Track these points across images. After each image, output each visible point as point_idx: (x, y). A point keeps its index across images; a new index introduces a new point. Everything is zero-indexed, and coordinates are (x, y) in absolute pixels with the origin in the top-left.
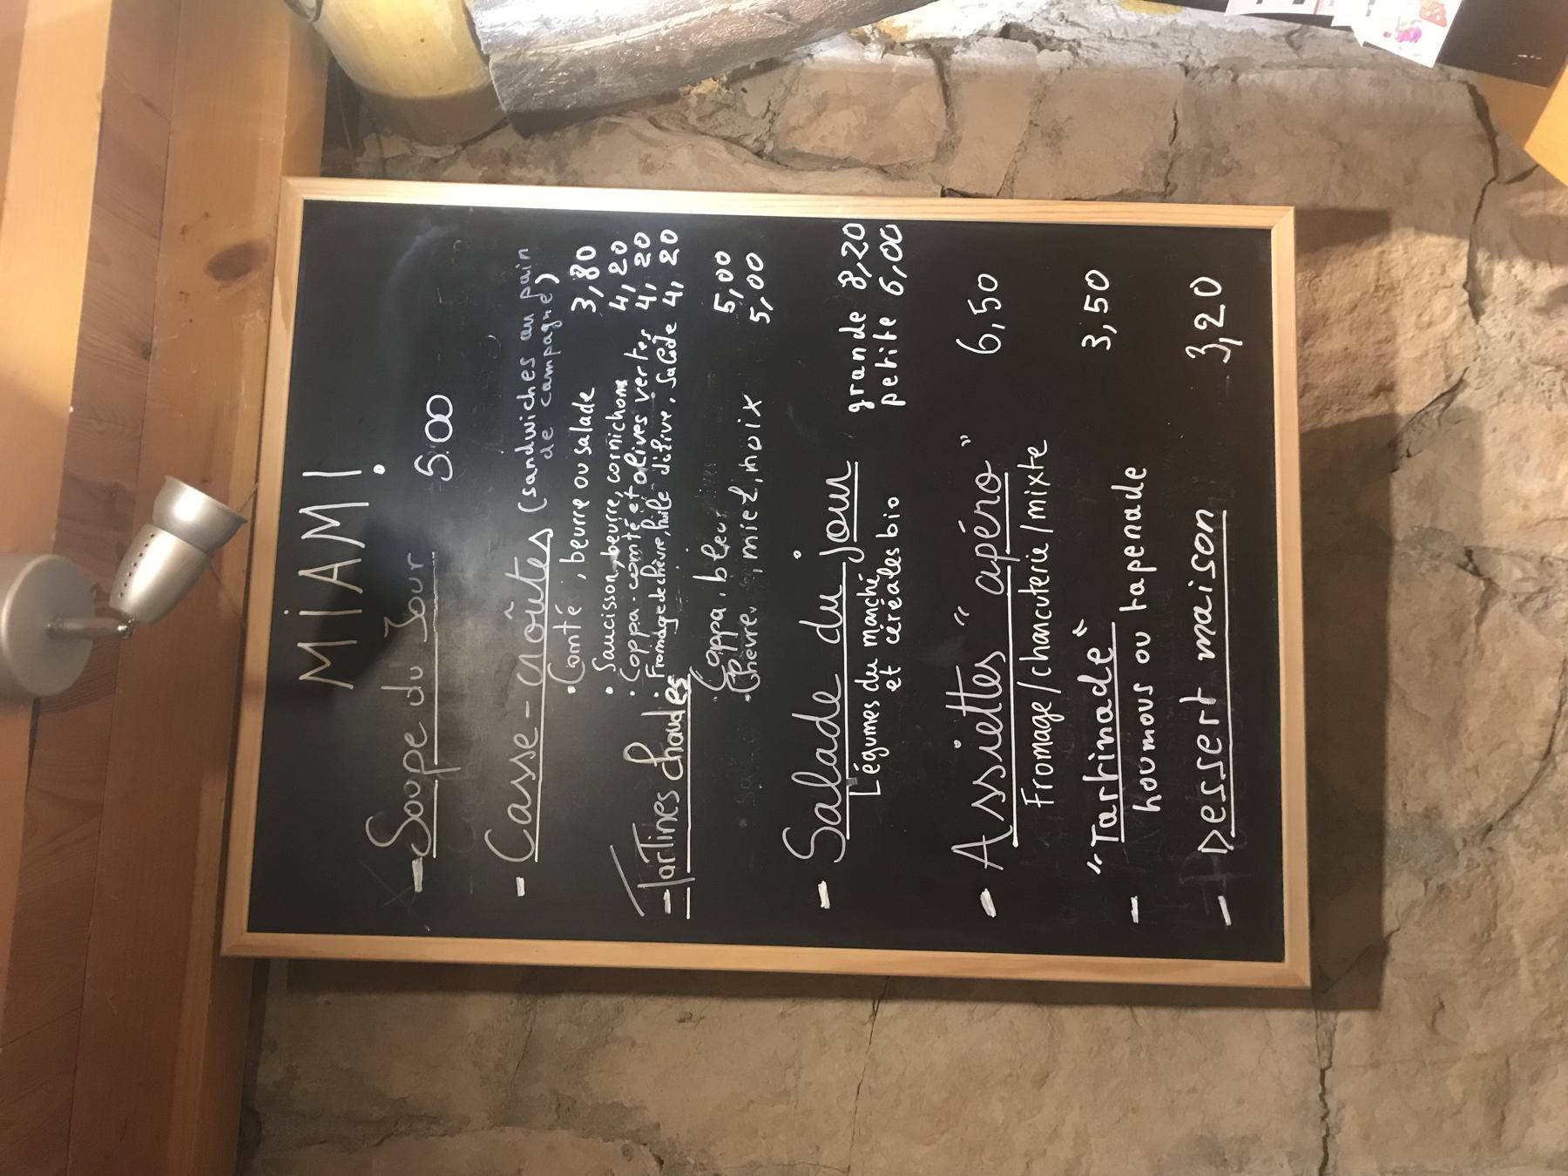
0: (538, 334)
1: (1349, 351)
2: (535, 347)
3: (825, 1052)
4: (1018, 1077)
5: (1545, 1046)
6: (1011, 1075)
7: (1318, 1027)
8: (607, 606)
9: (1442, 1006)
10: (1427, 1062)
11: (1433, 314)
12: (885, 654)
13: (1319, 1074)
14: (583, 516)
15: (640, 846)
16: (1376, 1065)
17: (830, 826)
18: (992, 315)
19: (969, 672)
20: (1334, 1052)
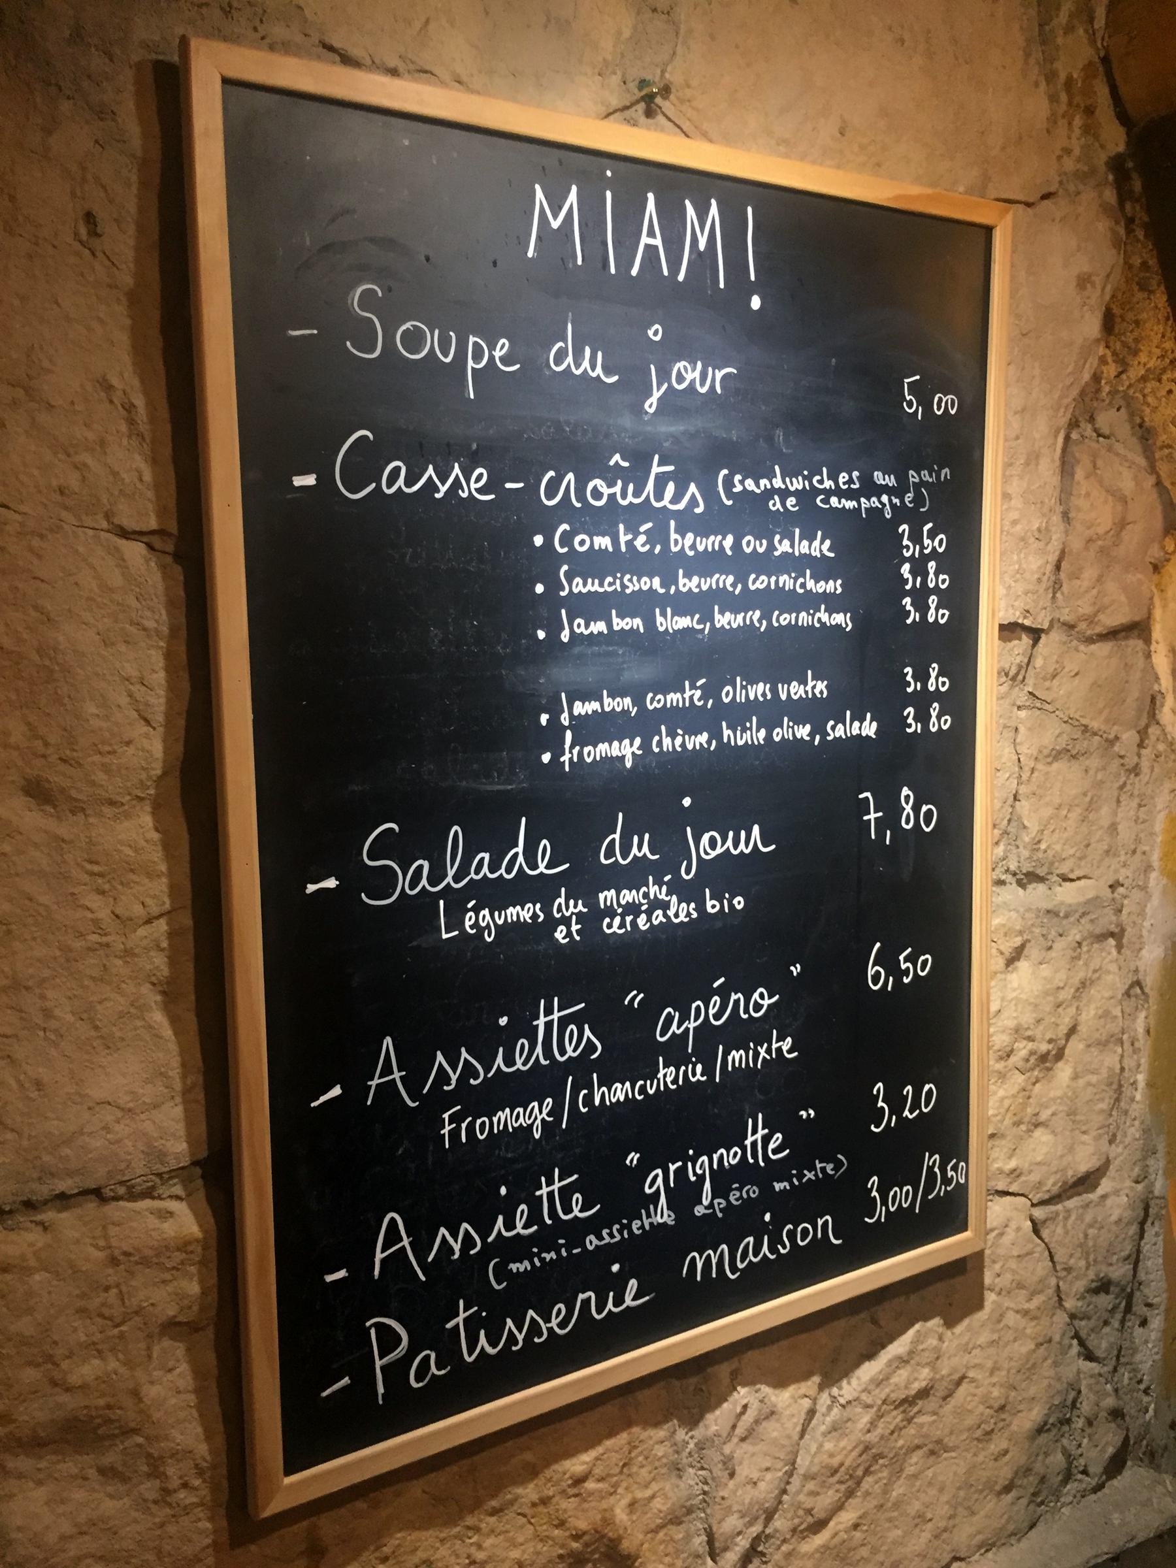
0: (880, 490)
2: (870, 489)
4: (44, 756)
5: (156, 1471)
10: (123, 1328)
12: (593, 917)
16: (114, 1261)
17: (403, 883)
18: (899, 974)
19: (577, 1019)
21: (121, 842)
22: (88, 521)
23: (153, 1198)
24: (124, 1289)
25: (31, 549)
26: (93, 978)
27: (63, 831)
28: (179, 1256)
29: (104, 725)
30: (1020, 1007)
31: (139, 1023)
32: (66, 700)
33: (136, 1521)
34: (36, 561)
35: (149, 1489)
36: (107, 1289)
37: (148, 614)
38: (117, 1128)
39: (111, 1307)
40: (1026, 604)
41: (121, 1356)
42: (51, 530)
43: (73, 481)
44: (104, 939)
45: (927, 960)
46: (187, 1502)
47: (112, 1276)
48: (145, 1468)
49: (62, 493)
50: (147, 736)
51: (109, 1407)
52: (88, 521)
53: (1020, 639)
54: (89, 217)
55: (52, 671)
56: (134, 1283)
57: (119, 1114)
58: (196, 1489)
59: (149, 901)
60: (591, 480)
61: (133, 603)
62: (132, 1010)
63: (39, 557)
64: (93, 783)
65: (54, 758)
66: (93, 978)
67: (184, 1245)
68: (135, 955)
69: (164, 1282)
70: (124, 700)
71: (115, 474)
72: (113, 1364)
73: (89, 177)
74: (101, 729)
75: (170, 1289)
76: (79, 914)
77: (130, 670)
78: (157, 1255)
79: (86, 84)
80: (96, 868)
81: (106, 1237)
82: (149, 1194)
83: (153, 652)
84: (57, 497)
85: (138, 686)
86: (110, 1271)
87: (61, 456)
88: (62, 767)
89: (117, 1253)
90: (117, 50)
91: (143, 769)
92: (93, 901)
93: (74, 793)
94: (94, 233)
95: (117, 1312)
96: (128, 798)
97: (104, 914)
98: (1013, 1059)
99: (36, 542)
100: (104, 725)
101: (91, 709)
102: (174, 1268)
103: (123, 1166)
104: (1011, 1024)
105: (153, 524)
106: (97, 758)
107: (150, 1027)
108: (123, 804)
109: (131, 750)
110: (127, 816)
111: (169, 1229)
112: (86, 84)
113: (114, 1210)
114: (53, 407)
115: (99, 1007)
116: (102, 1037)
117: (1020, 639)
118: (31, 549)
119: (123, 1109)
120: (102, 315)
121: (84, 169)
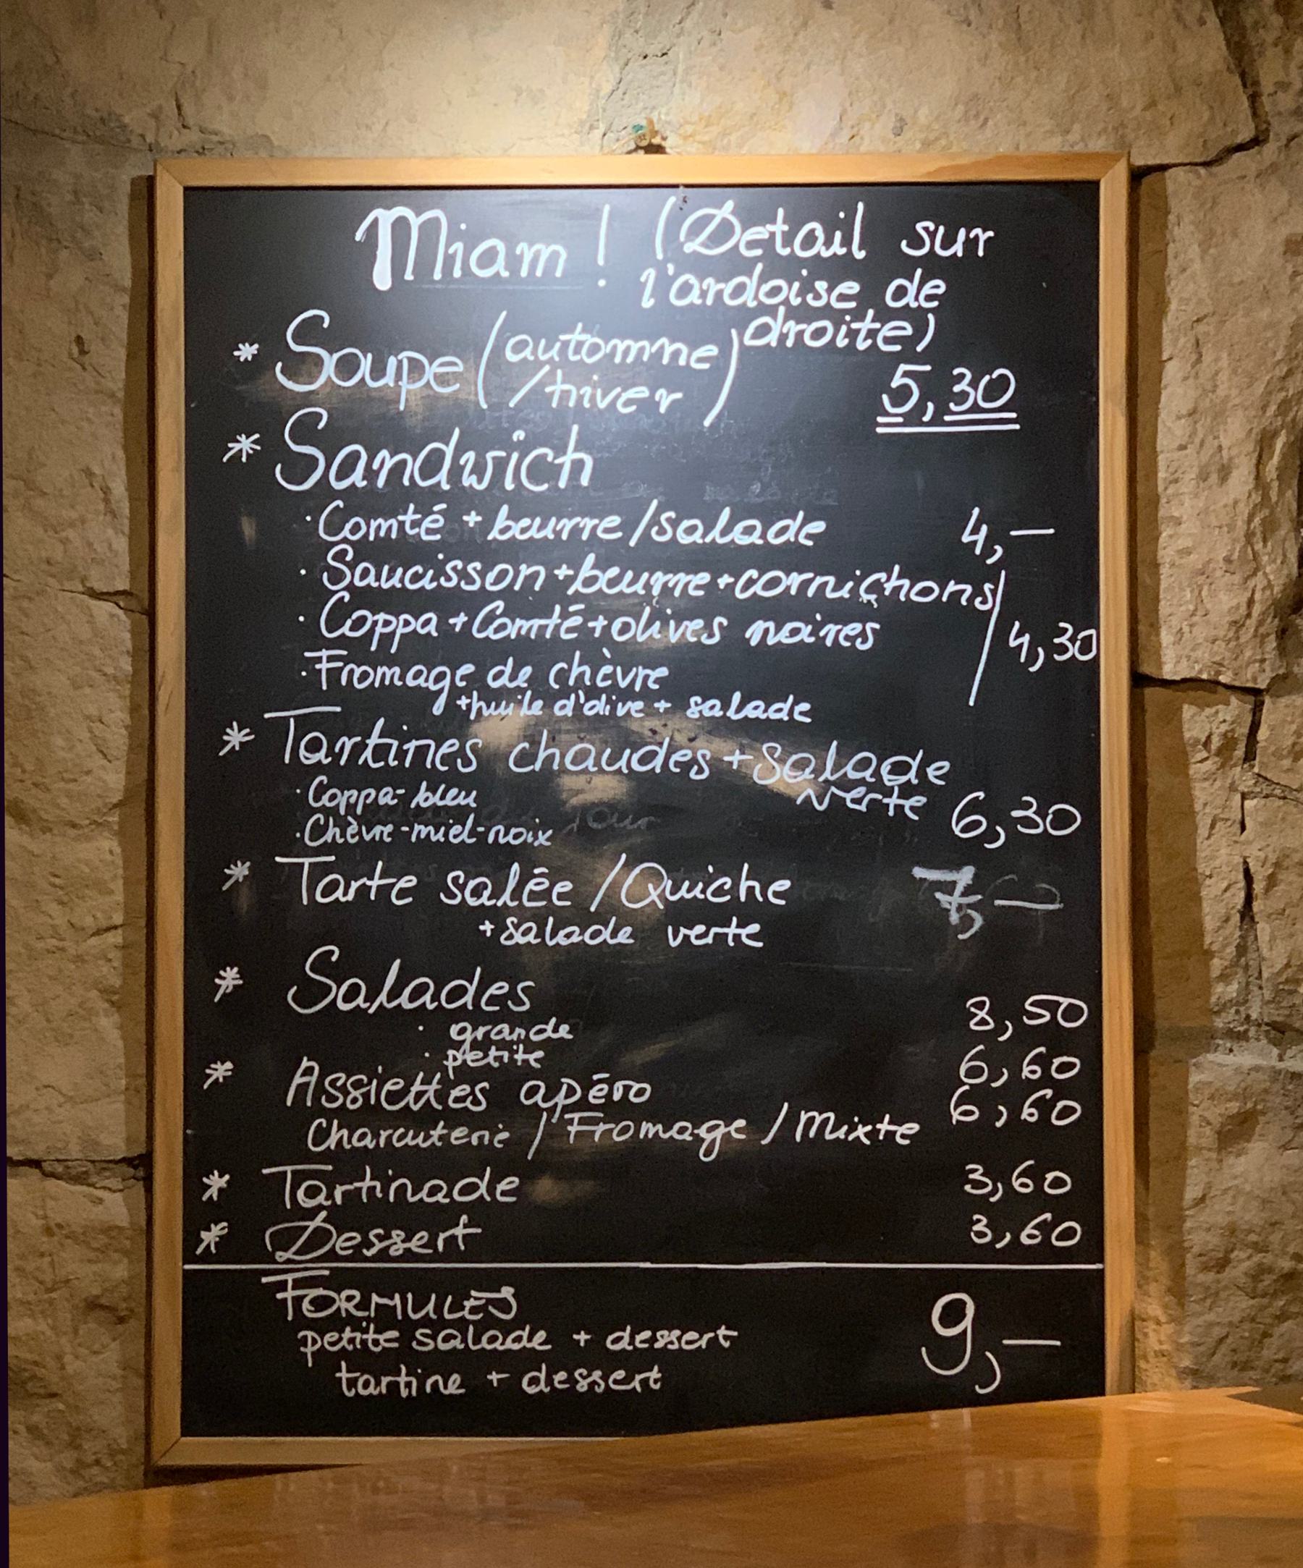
1: (1205, 80)
3: (46, 531)
4: (22, 781)
5: (74, 1444)
6: (24, 771)
7: (93, 1162)
8: (668, 520)
9: (121, 1320)
10: (54, 1295)
11: (1246, 579)
13: (35, 1157)
14: (810, 593)
15: (289, 1169)
16: (48, 1231)
20: (62, 1183)
21: (79, 861)
22: (67, 586)
23: (89, 1185)
24: (55, 1257)
25: (20, 609)
26: (50, 978)
27: (34, 847)
28: (103, 1239)
29: (69, 756)
30: (1241, 1200)
31: (87, 1025)
32: (40, 735)
33: (53, 1485)
34: (25, 619)
35: (68, 1459)
36: (42, 1255)
37: (108, 661)
38: (58, 1110)
39: (44, 1272)
40: (1213, 654)
41: (50, 1321)
42: (38, 594)
43: (58, 554)
44: (61, 944)
45: (1074, 1110)
46: (98, 1479)
47: (45, 1243)
48: (66, 1437)
49: (48, 562)
50: (103, 768)
51: (36, 1363)
52: (67, 586)
53: (1227, 703)
54: (79, 340)
55: (30, 710)
56: (64, 1255)
57: (62, 1100)
58: (107, 1468)
59: (99, 915)
60: (776, 546)
61: (97, 652)
62: (82, 1012)
63: (27, 616)
64: (58, 806)
65: (28, 783)
66: (50, 978)
67: (109, 1230)
68: (83, 961)
69: (89, 1261)
70: (85, 735)
71: (90, 545)
72: (43, 1326)
73: (81, 307)
74: (64, 759)
75: (95, 1268)
76: (42, 919)
77: (92, 710)
78: (84, 1233)
79: (79, 235)
80: (57, 881)
81: (43, 1208)
82: (80, 1179)
83: (111, 694)
84: (44, 566)
85: (98, 724)
86: (45, 1239)
87: (51, 533)
88: (34, 791)
89: (52, 1224)
90: (106, 204)
91: (99, 796)
92: (54, 908)
93: (42, 813)
94: (83, 352)
95: (48, 1277)
96: (87, 822)
97: (60, 921)
98: (1229, 1273)
99: (25, 604)
100: (69, 756)
101: (59, 741)
102: (98, 1249)
103: (59, 1145)
104: (1222, 1220)
105: (122, 584)
106: (62, 785)
107: (96, 1030)
108: (82, 827)
109: (89, 779)
110: (88, 839)
111: (97, 1213)
112: (79, 235)
113: (51, 1184)
114: (45, 494)
115: (52, 1002)
116: (53, 1030)
117: (1227, 703)
118: (20, 609)
119: (64, 1095)
120: (90, 416)
121: (77, 302)
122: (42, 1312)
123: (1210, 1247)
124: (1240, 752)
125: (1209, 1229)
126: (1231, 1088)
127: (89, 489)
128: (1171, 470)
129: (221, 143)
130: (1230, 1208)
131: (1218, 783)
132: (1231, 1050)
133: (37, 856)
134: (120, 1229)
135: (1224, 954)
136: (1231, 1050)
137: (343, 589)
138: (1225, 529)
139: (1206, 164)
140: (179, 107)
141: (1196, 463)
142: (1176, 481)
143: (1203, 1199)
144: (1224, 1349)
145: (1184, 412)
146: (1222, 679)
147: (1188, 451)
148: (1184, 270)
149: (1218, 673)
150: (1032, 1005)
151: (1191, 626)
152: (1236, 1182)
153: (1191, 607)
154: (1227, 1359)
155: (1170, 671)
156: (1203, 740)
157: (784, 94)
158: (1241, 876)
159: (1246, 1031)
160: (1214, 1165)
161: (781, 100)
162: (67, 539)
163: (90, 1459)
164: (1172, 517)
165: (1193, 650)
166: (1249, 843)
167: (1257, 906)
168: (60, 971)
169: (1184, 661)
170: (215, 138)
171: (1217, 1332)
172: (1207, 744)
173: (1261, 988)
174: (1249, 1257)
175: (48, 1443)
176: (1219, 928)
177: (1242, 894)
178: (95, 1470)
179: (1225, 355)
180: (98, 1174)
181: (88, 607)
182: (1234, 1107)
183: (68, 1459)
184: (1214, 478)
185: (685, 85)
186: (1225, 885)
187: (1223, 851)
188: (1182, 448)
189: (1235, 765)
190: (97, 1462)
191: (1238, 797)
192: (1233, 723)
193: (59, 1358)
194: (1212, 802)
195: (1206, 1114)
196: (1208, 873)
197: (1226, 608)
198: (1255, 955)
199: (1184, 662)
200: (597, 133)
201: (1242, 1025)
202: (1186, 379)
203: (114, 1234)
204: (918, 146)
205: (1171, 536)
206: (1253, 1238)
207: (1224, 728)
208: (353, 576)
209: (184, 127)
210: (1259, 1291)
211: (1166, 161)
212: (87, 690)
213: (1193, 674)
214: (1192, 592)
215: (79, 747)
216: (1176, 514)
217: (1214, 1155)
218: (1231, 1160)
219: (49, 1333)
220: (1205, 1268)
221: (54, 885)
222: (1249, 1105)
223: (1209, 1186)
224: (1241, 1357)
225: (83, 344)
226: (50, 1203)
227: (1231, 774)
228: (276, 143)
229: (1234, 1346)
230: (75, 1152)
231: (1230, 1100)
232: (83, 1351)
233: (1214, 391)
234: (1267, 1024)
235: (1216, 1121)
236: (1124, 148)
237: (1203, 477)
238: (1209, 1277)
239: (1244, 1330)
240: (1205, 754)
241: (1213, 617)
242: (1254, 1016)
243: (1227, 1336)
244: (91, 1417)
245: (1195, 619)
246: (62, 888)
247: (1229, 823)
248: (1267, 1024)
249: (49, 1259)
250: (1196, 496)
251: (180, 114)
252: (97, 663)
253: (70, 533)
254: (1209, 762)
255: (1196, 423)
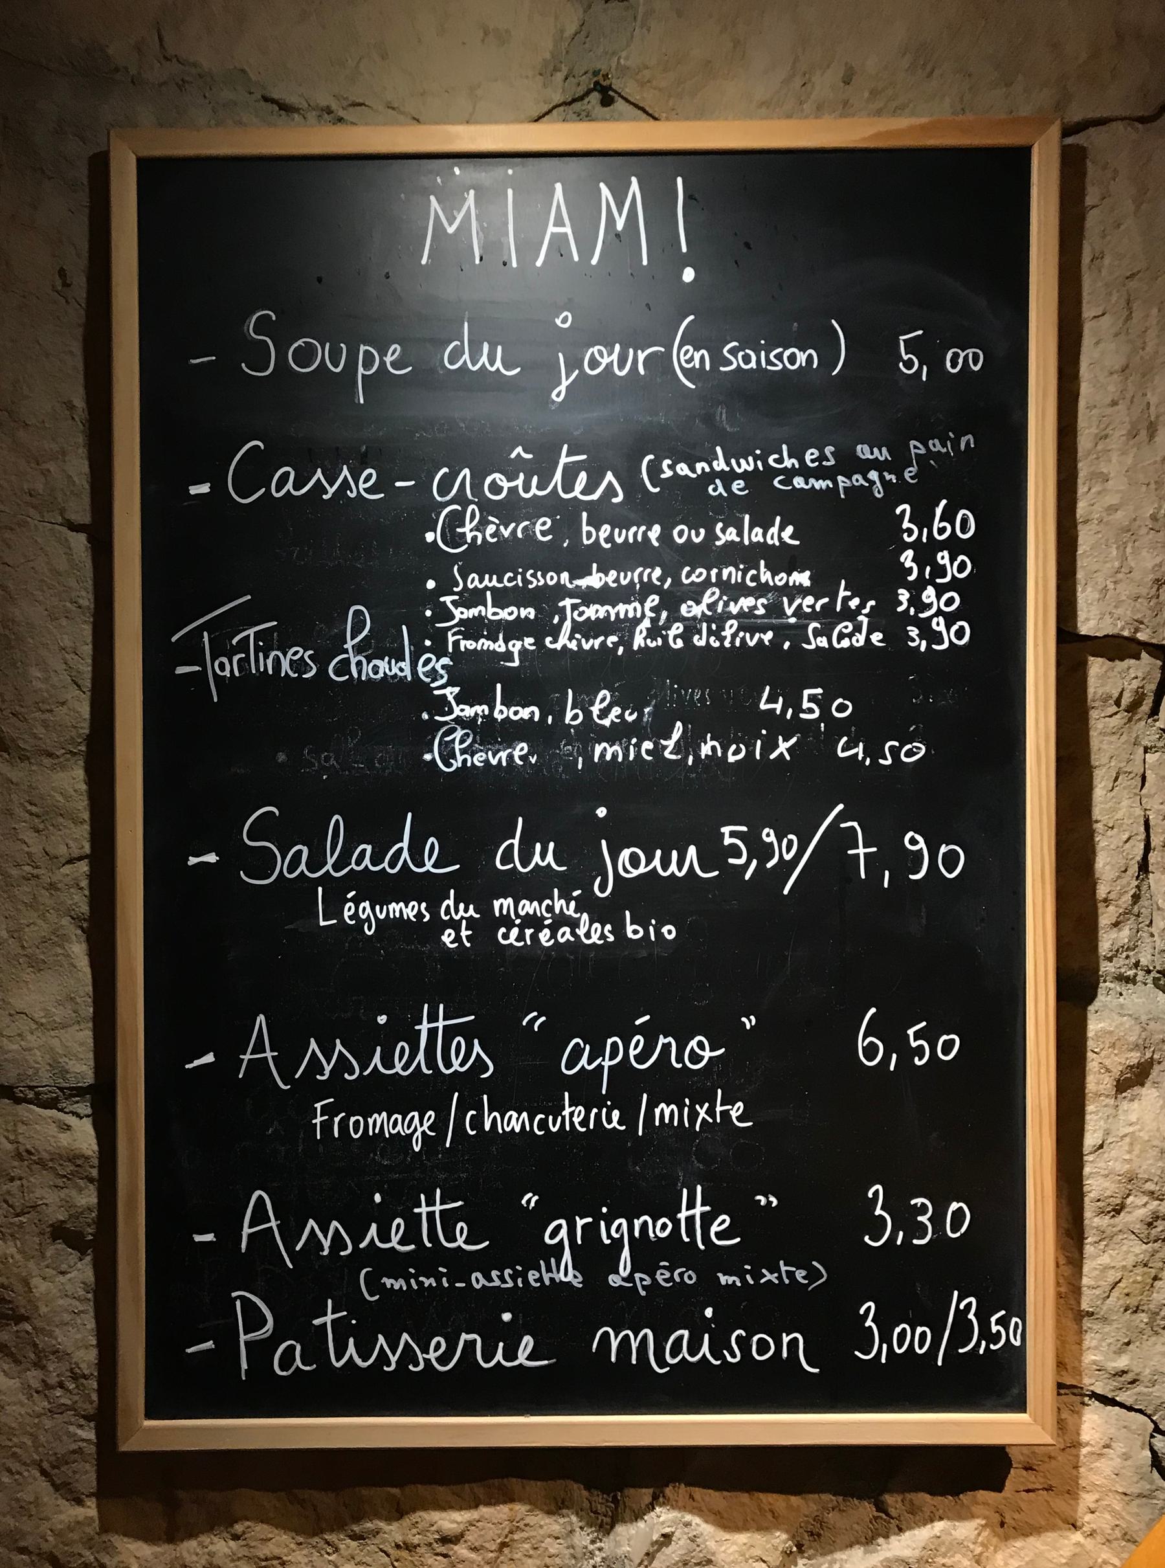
21: (53, 789)
22: (47, 517)
23: (59, 1110)
29: (43, 686)
36: (12, 1180)
38: (29, 1037)
39: (12, 1195)
43: (40, 487)
44: (35, 872)
49: (31, 495)
54: (62, 273)
57: (34, 1026)
58: (70, 1392)
63: (9, 547)
64: (35, 737)
67: (75, 1158)
68: (57, 889)
74: (40, 689)
78: (52, 1160)
80: (34, 809)
82: (51, 1104)
84: (28, 498)
85: (73, 656)
86: (16, 1163)
88: (13, 720)
89: (22, 1149)
92: (29, 836)
95: (17, 1203)
100: (43, 686)
101: (36, 672)
103: (30, 1072)
107: (69, 956)
109: (64, 709)
110: (63, 768)
111: (64, 1139)
119: (37, 1023)
122: (12, 1236)
123: (1108, 1193)
124: (1146, 707)
125: (1106, 1176)
126: (1132, 1039)
127: (70, 422)
128: (1102, 426)
129: (200, 76)
130: (1127, 1157)
131: (1124, 737)
132: (1121, 994)
133: (17, 784)
134: (87, 1158)
135: (1120, 902)
136: (1121, 994)
137: (738, 364)
138: (1153, 486)
139: (1142, 120)
140: (161, 39)
141: (1127, 419)
142: (1106, 437)
143: (1101, 1146)
144: (1115, 1293)
145: (1117, 367)
146: (1141, 636)
147: (1119, 407)
148: (1119, 226)
149: (1137, 630)
150: (278, 491)
151: (1115, 583)
152: (1131, 1129)
153: (1117, 564)
154: (1121, 1302)
155: (1084, 629)
156: (1116, 695)
157: (737, 43)
158: (1142, 829)
159: (1136, 975)
160: (1111, 1111)
161: (735, 47)
162: (49, 471)
163: (53, 1380)
164: (1102, 473)
165: (1116, 607)
166: (1149, 796)
167: (1153, 858)
168: (35, 898)
169: (1107, 617)
170: (194, 71)
171: (1112, 1276)
172: (1118, 703)
173: (1152, 935)
174: (1145, 1205)
175: (17, 1362)
176: (1119, 877)
177: (1142, 846)
178: (58, 1392)
179: (1155, 311)
180: (66, 1099)
181: (67, 540)
182: (1134, 1058)
183: (34, 1377)
184: (1144, 433)
185: (644, 30)
186: (1126, 837)
187: (1125, 803)
188: (1114, 403)
189: (1140, 719)
190: (61, 1385)
191: (1141, 750)
192: (1144, 679)
193: (26, 1283)
194: (1118, 756)
195: (1107, 1062)
196: (1110, 825)
197: (1150, 565)
198: (1146, 903)
199: (1108, 620)
200: (560, 76)
201: (1131, 969)
202: (1116, 335)
203: (79, 1162)
204: (866, 94)
205: (1099, 493)
206: (1150, 1186)
207: (1135, 684)
208: (453, 627)
209: (166, 58)
210: (1152, 1237)
211: (1105, 114)
212: (64, 622)
213: (1115, 631)
214: (1118, 548)
215: (55, 679)
216: (1105, 471)
217: (1112, 1101)
218: (1125, 1105)
219: (18, 1257)
220: (1101, 1212)
221: (31, 814)
222: (1148, 1055)
223: (1107, 1133)
224: (1133, 1301)
225: (65, 276)
226: (21, 1129)
227: (1135, 728)
228: (253, 78)
229: (1126, 1291)
230: (45, 1078)
231: (1132, 1050)
232: (50, 1272)
233: (1143, 349)
234: (1158, 972)
235: (1116, 1073)
236: (1060, 106)
237: (1133, 434)
238: (1105, 1221)
239: (1137, 1274)
240: (1115, 709)
241: (1136, 575)
242: (1144, 962)
243: (1120, 1281)
244: (56, 1339)
245: (1120, 576)
246: (38, 816)
247: (1132, 775)
248: (1158, 972)
249: (19, 1182)
250: (1124, 453)
251: (161, 45)
252: (73, 594)
253: (52, 466)
254: (1118, 716)
255: (1127, 379)
